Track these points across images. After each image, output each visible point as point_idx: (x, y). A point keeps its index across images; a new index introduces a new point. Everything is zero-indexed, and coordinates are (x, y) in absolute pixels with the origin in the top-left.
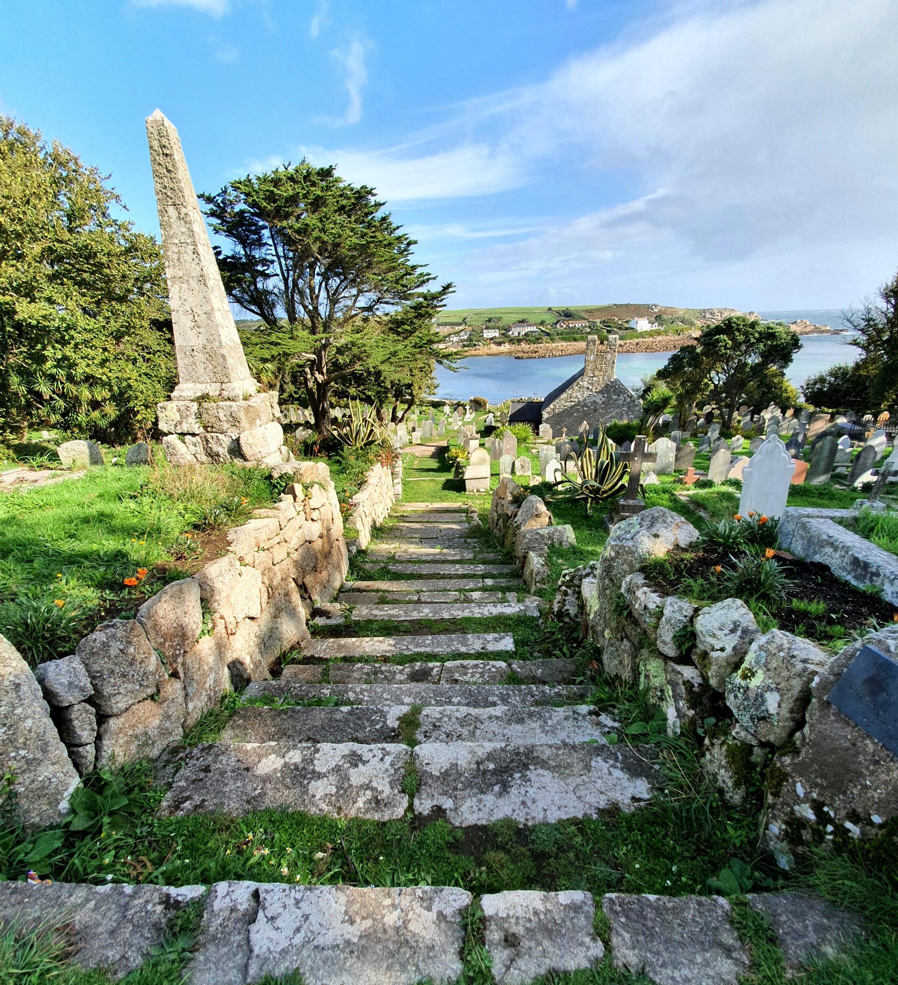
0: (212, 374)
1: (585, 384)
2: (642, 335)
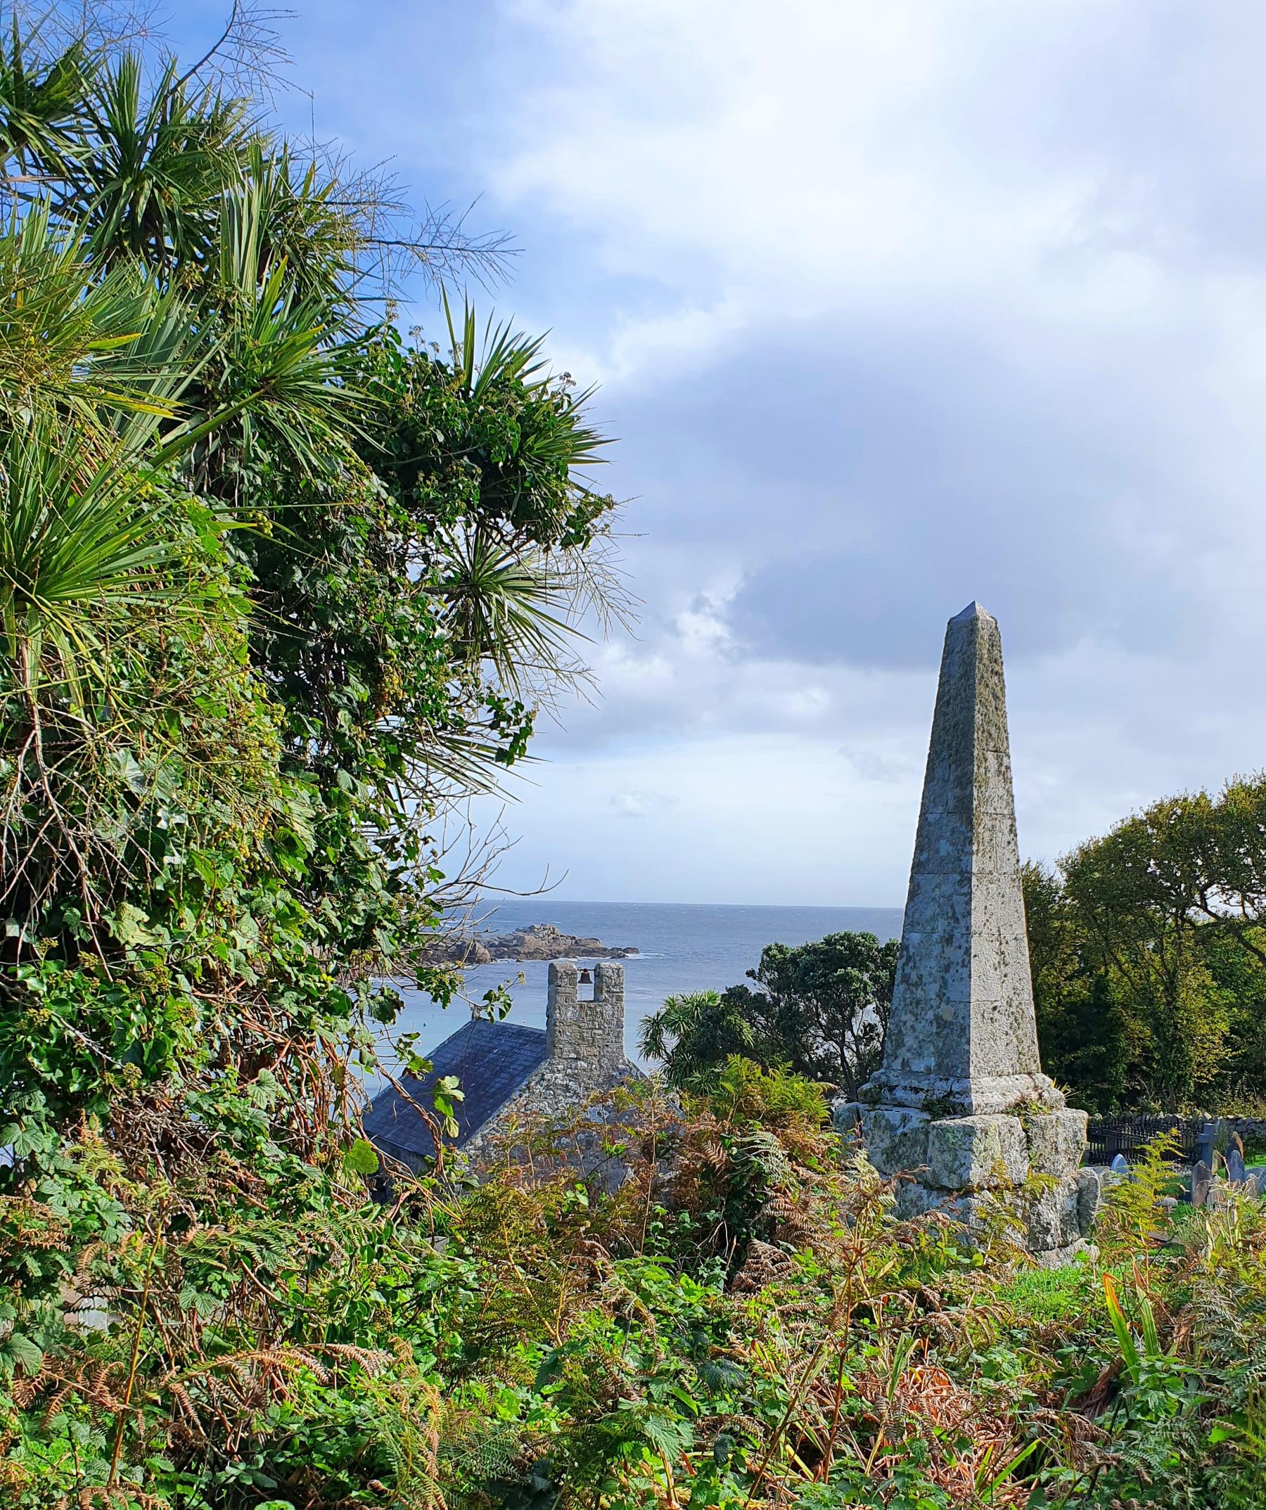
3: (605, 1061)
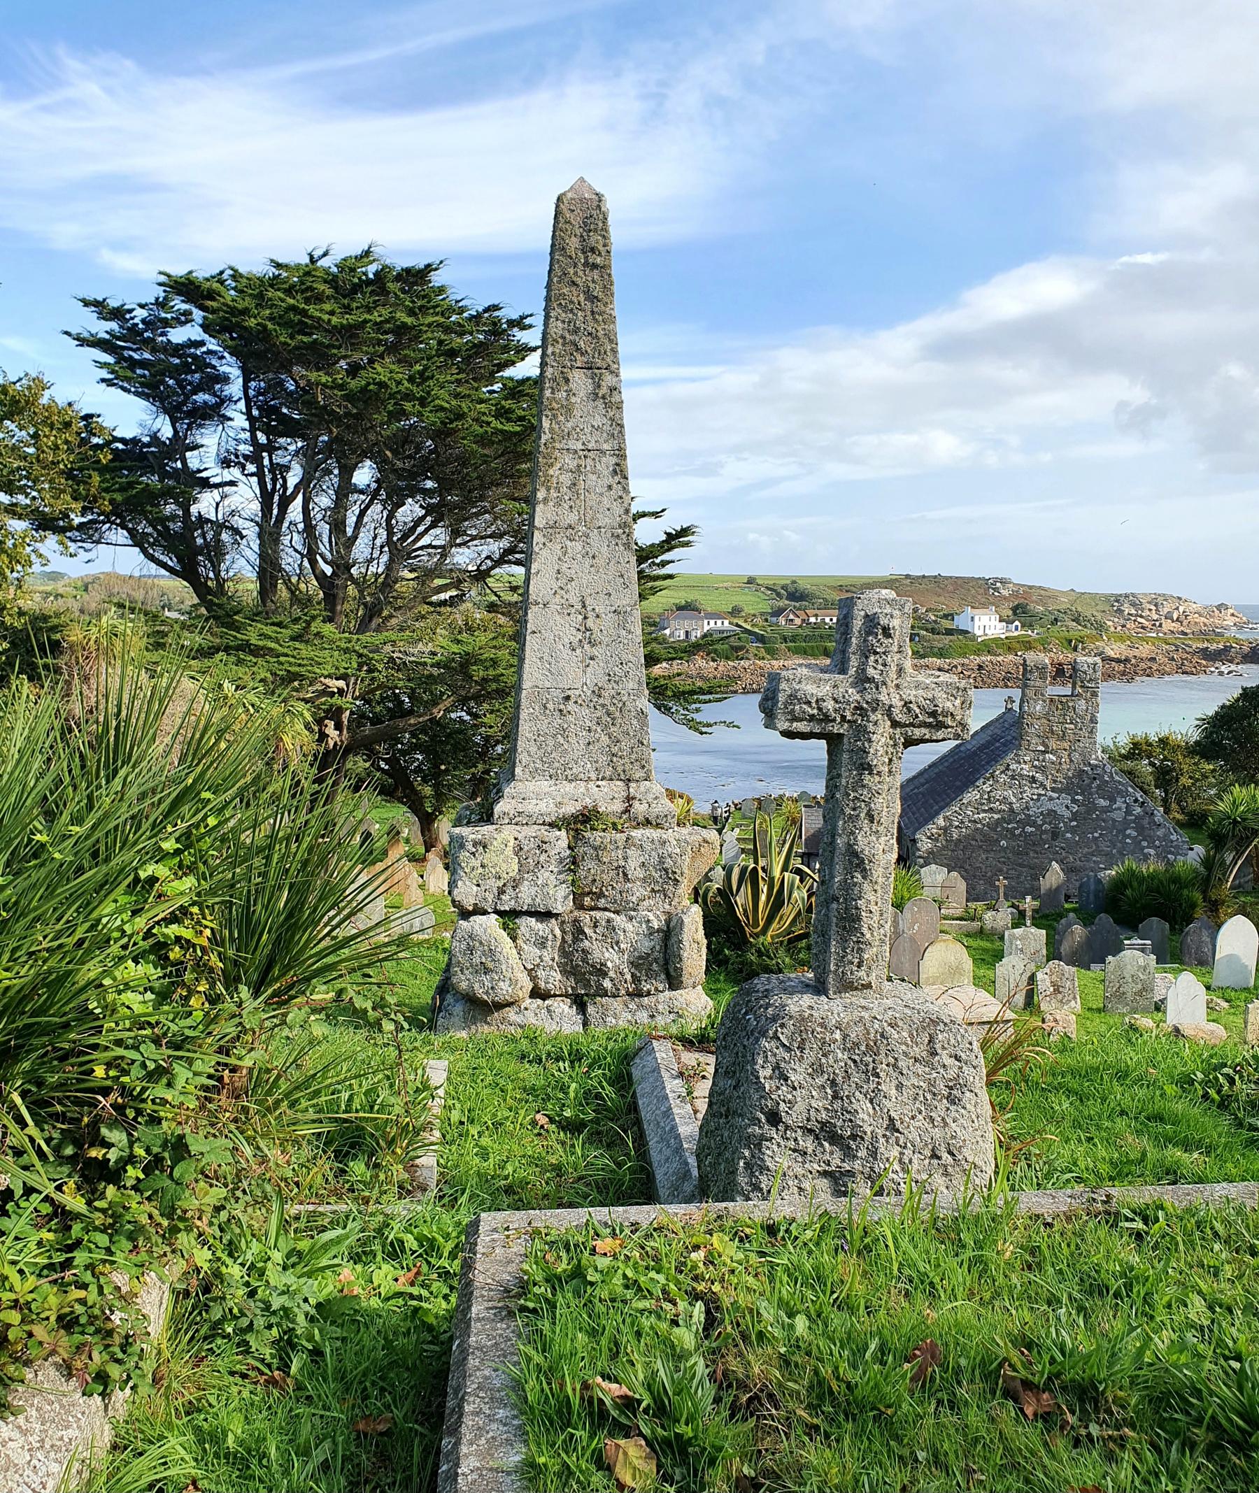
0: (604, 759)
1: (1026, 769)
2: (989, 646)
3: (1075, 756)
